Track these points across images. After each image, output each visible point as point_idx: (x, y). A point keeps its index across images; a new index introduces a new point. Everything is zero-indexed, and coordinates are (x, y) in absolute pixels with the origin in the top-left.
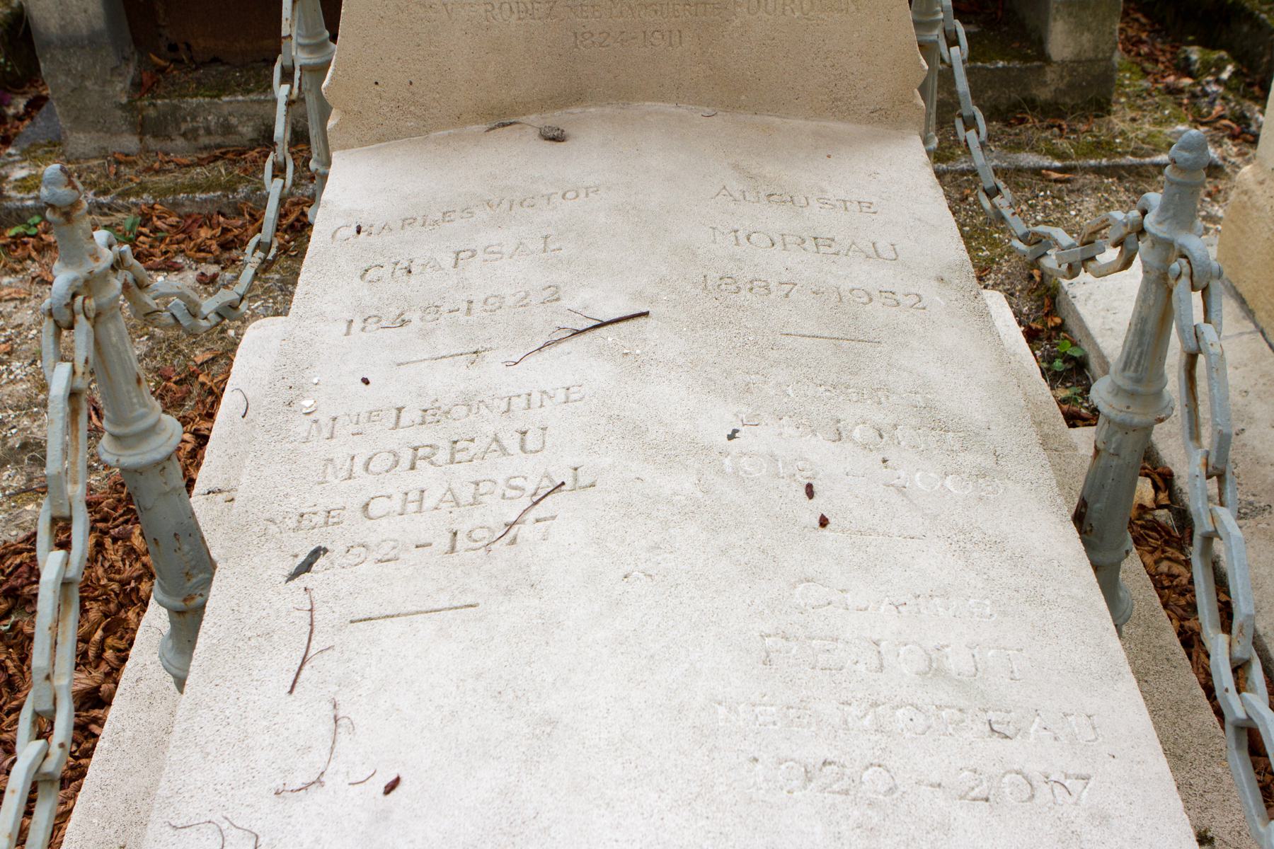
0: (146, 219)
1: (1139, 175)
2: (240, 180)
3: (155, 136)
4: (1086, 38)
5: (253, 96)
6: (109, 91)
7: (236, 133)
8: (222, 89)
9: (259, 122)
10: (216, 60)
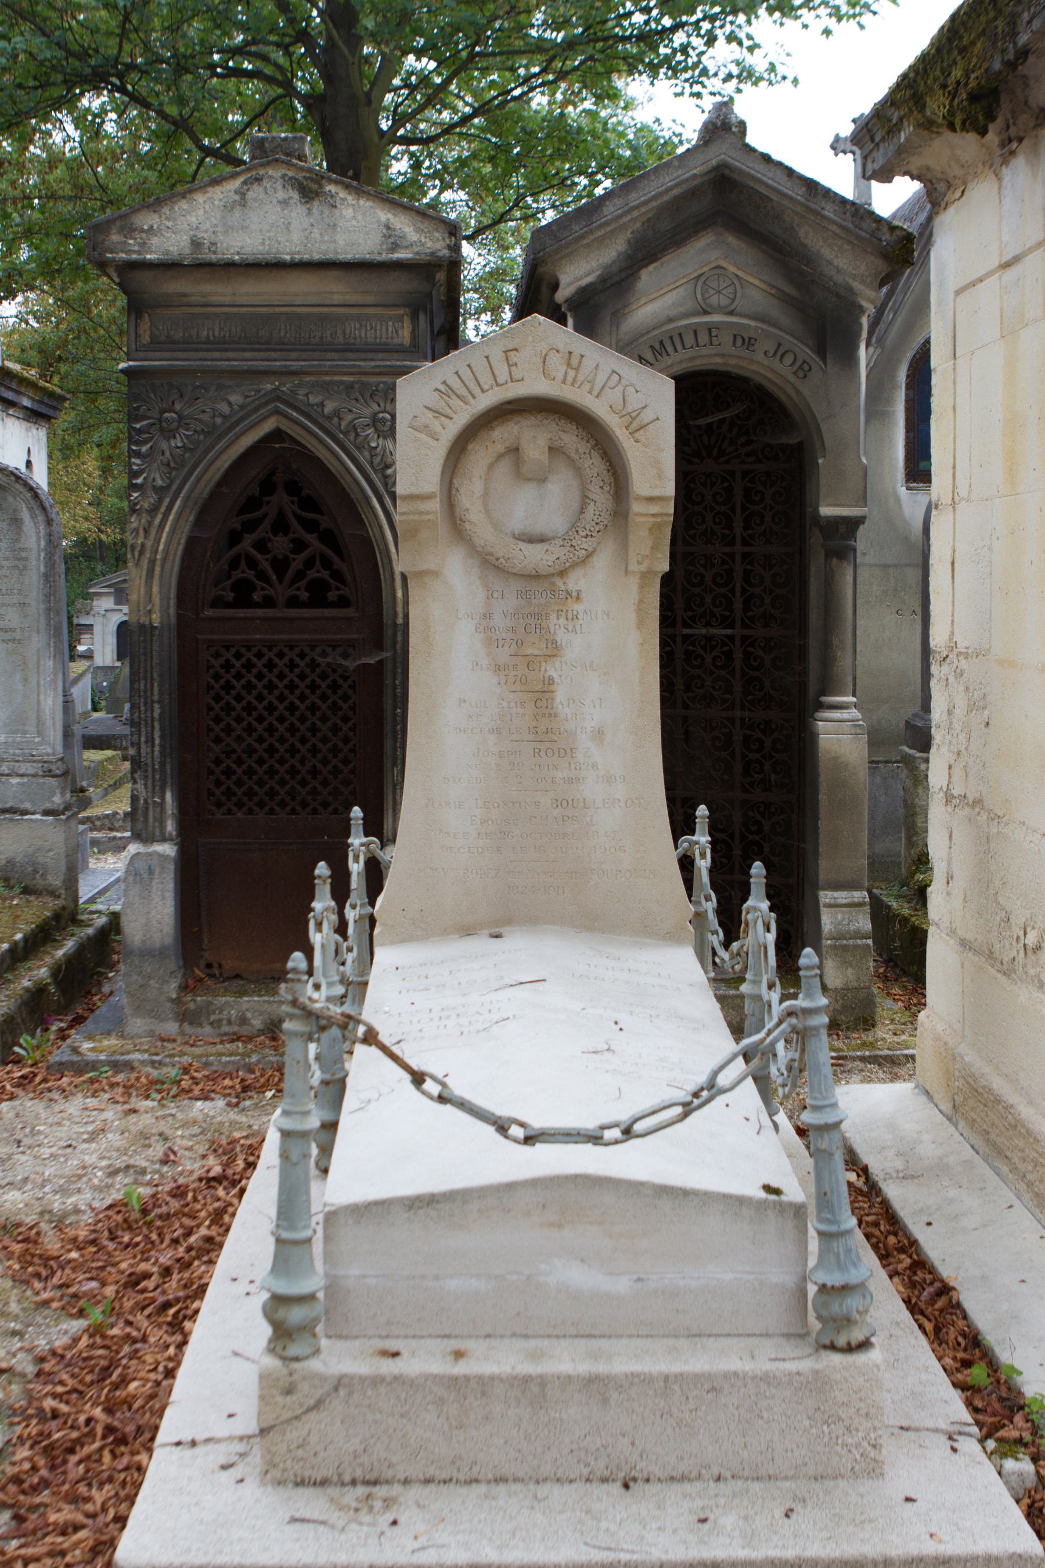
0: (186, 1070)
1: (893, 1062)
2: (252, 1051)
3: (191, 1023)
4: (850, 972)
5: (266, 998)
6: (166, 988)
7: (249, 1024)
8: (243, 993)
9: (266, 1017)
10: (238, 976)
